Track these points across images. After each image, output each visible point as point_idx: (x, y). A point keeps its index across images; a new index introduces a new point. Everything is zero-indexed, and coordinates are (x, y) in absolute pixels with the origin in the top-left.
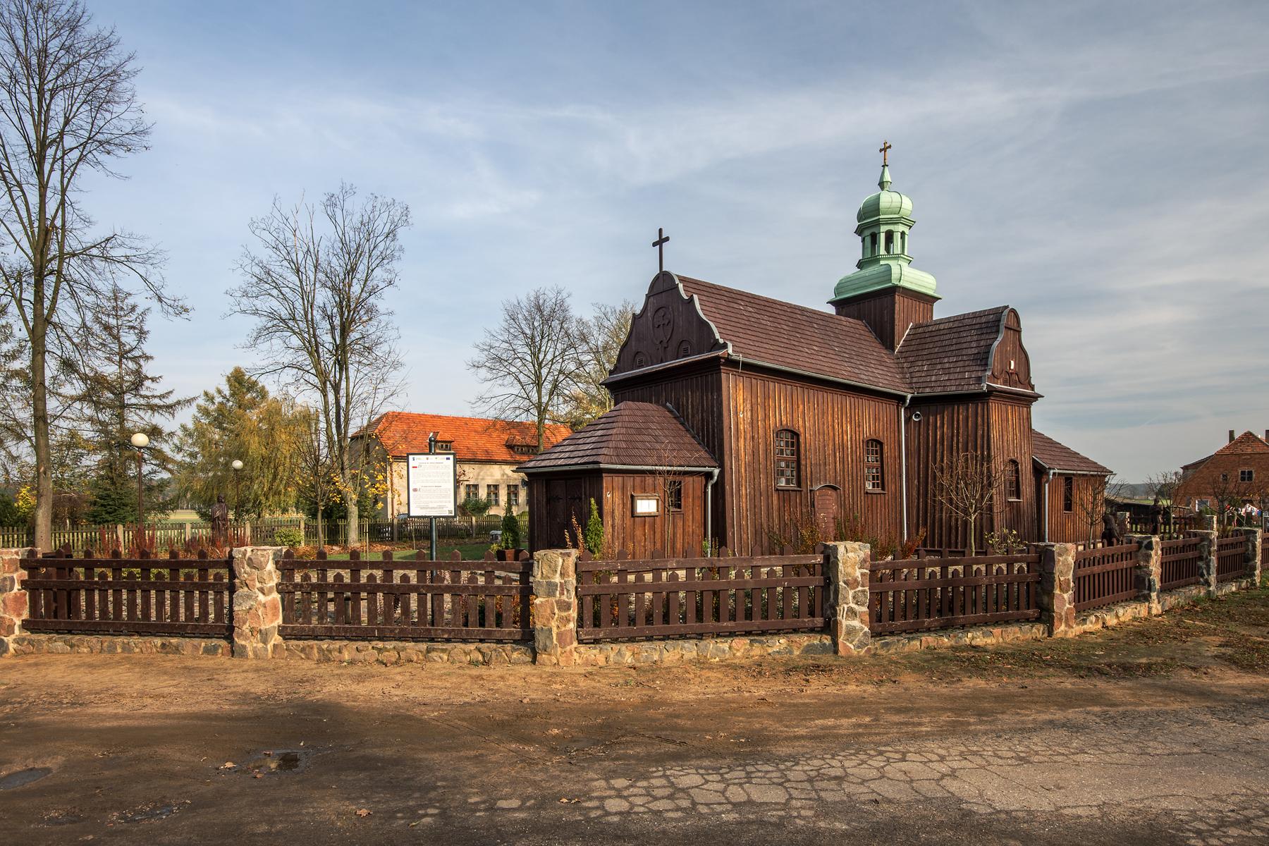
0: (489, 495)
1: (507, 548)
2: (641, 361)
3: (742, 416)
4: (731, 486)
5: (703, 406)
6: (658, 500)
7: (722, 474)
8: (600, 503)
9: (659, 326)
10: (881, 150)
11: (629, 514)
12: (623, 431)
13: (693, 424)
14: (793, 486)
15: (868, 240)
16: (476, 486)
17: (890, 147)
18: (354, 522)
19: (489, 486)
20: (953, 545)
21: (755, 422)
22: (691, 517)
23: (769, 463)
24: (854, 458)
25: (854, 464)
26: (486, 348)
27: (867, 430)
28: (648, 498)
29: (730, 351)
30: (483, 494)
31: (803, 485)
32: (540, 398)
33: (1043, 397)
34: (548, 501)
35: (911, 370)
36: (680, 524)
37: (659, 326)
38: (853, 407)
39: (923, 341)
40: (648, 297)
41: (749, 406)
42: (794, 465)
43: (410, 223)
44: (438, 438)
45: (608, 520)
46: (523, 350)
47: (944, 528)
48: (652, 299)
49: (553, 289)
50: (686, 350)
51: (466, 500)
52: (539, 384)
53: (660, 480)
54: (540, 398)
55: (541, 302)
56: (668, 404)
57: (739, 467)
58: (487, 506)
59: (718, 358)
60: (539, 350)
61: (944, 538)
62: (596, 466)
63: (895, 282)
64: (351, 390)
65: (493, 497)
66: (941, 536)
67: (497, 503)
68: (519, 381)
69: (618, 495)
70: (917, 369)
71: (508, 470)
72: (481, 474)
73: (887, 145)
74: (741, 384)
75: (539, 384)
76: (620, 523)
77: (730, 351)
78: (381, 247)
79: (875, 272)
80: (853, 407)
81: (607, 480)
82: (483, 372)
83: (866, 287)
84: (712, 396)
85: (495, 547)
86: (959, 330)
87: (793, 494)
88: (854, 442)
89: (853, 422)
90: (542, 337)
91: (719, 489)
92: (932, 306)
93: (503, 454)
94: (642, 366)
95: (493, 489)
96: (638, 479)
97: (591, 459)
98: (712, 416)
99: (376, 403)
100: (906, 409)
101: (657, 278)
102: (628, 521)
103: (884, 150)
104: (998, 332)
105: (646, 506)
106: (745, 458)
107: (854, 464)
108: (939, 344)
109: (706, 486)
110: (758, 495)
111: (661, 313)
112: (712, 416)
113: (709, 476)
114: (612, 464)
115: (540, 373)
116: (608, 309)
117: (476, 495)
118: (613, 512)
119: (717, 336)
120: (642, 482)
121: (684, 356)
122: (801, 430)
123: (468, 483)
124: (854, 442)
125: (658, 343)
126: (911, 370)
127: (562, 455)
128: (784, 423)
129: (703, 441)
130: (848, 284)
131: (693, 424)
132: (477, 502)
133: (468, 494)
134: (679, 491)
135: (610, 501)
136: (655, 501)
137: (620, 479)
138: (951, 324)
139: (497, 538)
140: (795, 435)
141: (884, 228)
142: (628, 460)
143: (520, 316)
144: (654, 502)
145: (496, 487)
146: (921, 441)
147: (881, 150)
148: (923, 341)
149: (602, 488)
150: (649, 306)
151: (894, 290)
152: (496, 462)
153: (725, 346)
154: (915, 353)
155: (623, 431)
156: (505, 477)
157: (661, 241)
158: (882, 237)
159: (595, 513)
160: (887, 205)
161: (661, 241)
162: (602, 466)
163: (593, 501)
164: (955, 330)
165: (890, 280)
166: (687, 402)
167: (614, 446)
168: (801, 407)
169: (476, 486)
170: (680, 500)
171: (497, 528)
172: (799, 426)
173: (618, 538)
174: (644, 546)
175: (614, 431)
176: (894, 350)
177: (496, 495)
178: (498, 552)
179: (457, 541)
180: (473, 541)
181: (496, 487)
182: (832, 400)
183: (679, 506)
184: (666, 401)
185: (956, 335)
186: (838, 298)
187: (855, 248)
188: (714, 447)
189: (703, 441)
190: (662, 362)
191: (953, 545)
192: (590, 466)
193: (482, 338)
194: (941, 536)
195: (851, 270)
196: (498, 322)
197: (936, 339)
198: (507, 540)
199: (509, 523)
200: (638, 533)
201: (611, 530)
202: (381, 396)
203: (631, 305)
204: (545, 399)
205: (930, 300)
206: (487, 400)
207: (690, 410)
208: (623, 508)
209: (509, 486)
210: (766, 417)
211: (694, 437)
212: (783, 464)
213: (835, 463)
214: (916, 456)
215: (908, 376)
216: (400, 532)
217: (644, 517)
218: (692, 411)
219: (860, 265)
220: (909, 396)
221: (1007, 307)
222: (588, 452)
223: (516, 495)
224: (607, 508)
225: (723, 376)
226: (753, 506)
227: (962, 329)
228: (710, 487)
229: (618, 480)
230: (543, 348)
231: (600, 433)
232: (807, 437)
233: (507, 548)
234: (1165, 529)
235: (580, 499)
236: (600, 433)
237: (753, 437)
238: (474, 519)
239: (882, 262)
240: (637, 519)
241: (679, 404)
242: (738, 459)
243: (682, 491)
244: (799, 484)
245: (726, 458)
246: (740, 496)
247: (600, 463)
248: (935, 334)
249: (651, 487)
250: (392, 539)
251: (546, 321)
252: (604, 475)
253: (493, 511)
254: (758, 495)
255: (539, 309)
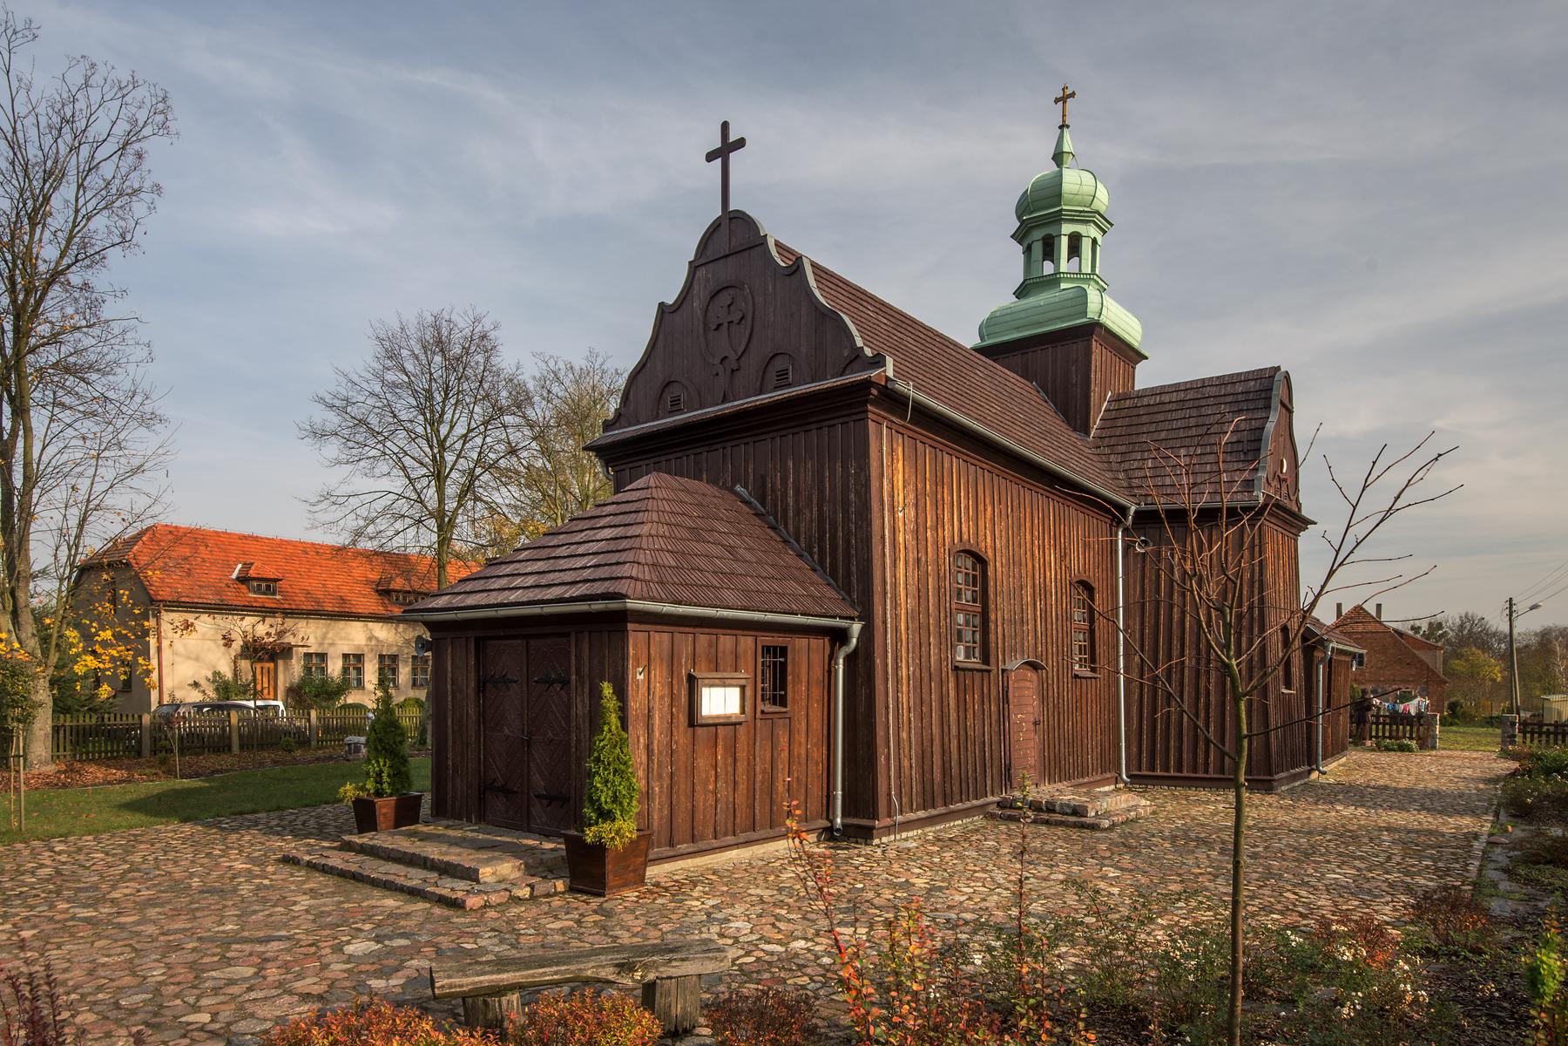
0: (345, 670)
1: (379, 793)
2: (676, 401)
3: (901, 515)
4: (884, 661)
5: (821, 492)
6: (743, 688)
7: (867, 634)
8: (621, 693)
9: (719, 326)
10: (1057, 101)
11: (683, 718)
12: (663, 530)
13: (797, 529)
14: (975, 662)
15: (1038, 249)
16: (323, 657)
17: (1073, 95)
18: (43, 722)
19: (346, 656)
20: (1201, 767)
21: (921, 529)
22: (804, 724)
23: (942, 615)
24: (1059, 612)
25: (1060, 623)
26: (338, 403)
27: (1078, 564)
28: (724, 683)
29: (890, 373)
30: (335, 668)
31: (992, 660)
32: (441, 501)
33: (1315, 523)
34: (481, 687)
35: (1126, 466)
36: (783, 740)
37: (719, 326)
38: (1057, 518)
39: (1135, 421)
40: (694, 267)
41: (912, 496)
42: (977, 621)
43: (173, 129)
44: (252, 573)
45: (637, 733)
46: (405, 407)
47: (1185, 739)
48: (701, 272)
49: (465, 312)
50: (783, 374)
51: (303, 679)
52: (439, 477)
53: (747, 642)
54: (441, 501)
55: (445, 332)
56: (738, 488)
57: (896, 617)
58: (343, 688)
59: (868, 383)
60: (441, 416)
61: (1185, 756)
62: (613, 605)
63: (1092, 313)
64: (36, 455)
65: (353, 674)
66: (1180, 750)
67: (360, 684)
68: (404, 468)
69: (659, 674)
70: (1136, 465)
71: (382, 632)
72: (330, 635)
73: (1068, 92)
74: (900, 449)
75: (439, 477)
76: (665, 740)
77: (890, 373)
78: (107, 170)
79: (1057, 300)
80: (1057, 518)
81: (636, 639)
82: (333, 448)
83: (1040, 324)
84: (845, 468)
85: (349, 790)
86: (1197, 403)
87: (978, 676)
88: (1059, 584)
89: (1058, 547)
90: (446, 394)
91: (862, 668)
92: (1134, 368)
93: (371, 604)
94: (680, 411)
95: (354, 661)
96: (703, 639)
97: (600, 588)
98: (846, 512)
99: (99, 487)
100: (1126, 531)
101: (715, 227)
102: (682, 735)
103: (1063, 99)
104: (1268, 407)
105: (720, 701)
106: (906, 603)
107: (1060, 623)
108: (1167, 426)
109: (832, 657)
110: (926, 680)
111: (725, 298)
112: (846, 512)
113: (840, 636)
114: (653, 599)
115: (442, 457)
116: (562, 366)
117: (323, 670)
118: (649, 716)
119: (859, 343)
120: (710, 646)
121: (777, 388)
122: (990, 553)
123: (305, 650)
124: (1059, 584)
125: (717, 361)
126: (1126, 466)
127: (518, 582)
128: (965, 537)
129: (822, 563)
130: (1008, 318)
131: (797, 529)
132: (324, 682)
133: (308, 669)
134: (784, 666)
135: (643, 690)
136: (737, 690)
137: (666, 637)
138: (1182, 395)
139: (357, 750)
140: (980, 560)
141: (1067, 229)
142: (685, 594)
143: (405, 353)
144: (735, 693)
145: (359, 658)
146: (1147, 587)
147: (1057, 101)
148: (1135, 421)
149: (625, 658)
150: (696, 286)
151: (1094, 329)
152: (357, 617)
153: (878, 361)
154: (1126, 440)
155: (663, 530)
156: (373, 642)
157: (726, 149)
158: (1064, 241)
159: (613, 719)
160: (1074, 188)
161: (726, 149)
162: (632, 604)
163: (607, 689)
164: (1191, 404)
165: (1085, 313)
166: (784, 479)
167: (650, 561)
168: (989, 509)
169: (323, 657)
170: (784, 686)
171: (359, 731)
172: (986, 547)
173: (660, 776)
174: (715, 792)
175: (645, 529)
176: (1087, 433)
177: (359, 671)
178: (358, 802)
179: (280, 755)
180: (310, 755)
181: (359, 658)
182: (1042, 507)
183: (782, 701)
184: (735, 481)
185: (1194, 412)
186: (989, 342)
187: (1011, 263)
188: (848, 575)
189: (822, 563)
190: (724, 400)
191: (1201, 767)
192: (598, 606)
193: (331, 385)
194: (1180, 750)
195: (1009, 300)
196: (362, 359)
197: (1161, 417)
198: (379, 774)
199: (386, 732)
200: (702, 762)
201: (644, 758)
202: (107, 473)
203: (600, 360)
204: (451, 505)
205: (1131, 356)
206: (341, 500)
207: (791, 501)
208: (671, 706)
209: (382, 657)
210: (938, 521)
211: (800, 556)
212: (961, 618)
213: (1036, 621)
214: (1138, 613)
215: (1121, 476)
216: (155, 740)
217: (717, 724)
218: (796, 501)
219: (1021, 292)
220: (1133, 509)
221: (1278, 368)
222: (586, 574)
223: (394, 671)
224: (636, 704)
225: (871, 425)
226: (918, 701)
227: (1203, 402)
228: (841, 661)
229: (660, 639)
230: (448, 417)
231: (607, 533)
232: (998, 569)
233: (379, 793)
234: (1391, 731)
235: (565, 683)
236: (607, 533)
237: (919, 560)
238: (313, 714)
239: (1063, 286)
240: (699, 731)
241: (764, 486)
242: (895, 606)
243: (789, 668)
244: (986, 659)
245: (877, 599)
246: (898, 681)
247: (625, 596)
248: (1155, 409)
249: (730, 659)
250: (139, 754)
251: (455, 364)
252: (630, 626)
253: (352, 698)
254: (926, 680)
255: (441, 345)
